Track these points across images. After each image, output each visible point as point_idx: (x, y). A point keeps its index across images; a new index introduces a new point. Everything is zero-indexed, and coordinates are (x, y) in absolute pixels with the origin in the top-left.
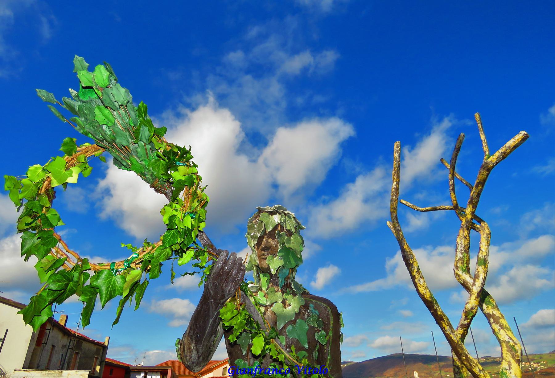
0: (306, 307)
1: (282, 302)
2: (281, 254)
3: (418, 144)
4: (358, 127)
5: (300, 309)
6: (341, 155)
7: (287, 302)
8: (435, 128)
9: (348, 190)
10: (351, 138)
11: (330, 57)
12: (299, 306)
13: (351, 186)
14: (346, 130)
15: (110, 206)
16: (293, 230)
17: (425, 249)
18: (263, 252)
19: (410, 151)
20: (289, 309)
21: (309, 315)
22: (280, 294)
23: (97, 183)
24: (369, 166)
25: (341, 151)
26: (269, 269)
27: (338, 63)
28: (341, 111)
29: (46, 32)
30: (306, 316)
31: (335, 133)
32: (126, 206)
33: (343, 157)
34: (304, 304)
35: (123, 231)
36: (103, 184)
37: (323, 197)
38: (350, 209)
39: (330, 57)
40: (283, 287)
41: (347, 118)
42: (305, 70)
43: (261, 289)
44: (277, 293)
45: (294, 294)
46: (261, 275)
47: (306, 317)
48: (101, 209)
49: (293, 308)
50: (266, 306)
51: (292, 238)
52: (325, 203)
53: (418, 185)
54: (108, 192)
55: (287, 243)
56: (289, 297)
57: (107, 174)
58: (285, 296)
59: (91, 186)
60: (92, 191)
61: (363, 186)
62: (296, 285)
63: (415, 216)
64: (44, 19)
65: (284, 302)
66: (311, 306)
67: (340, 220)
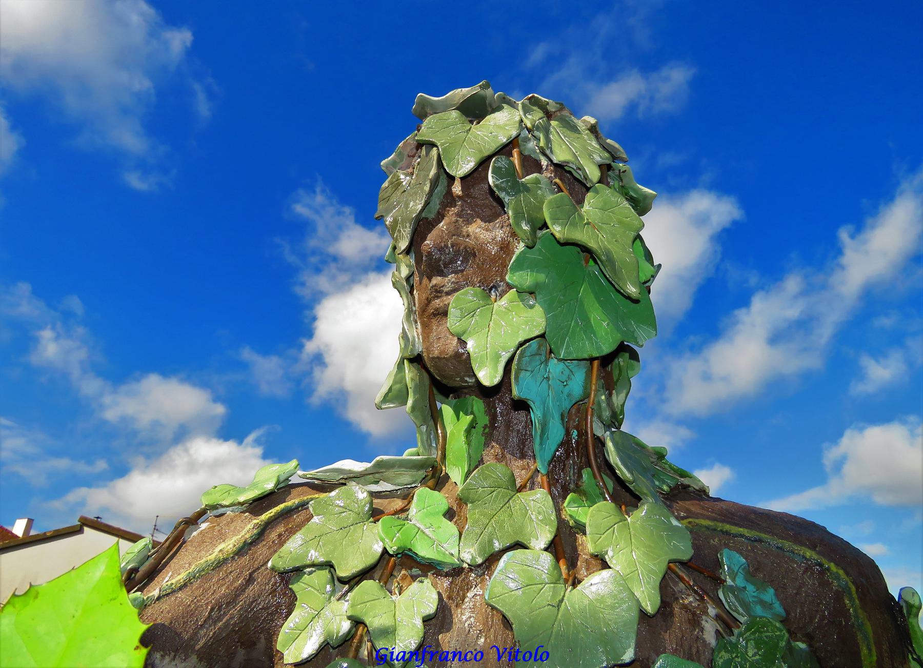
0: (695, 571)
1: (552, 547)
2: (524, 278)
3: (869, 221)
4: (745, 203)
5: (665, 587)
6: (719, 256)
7: (588, 545)
8: (905, 185)
9: (737, 322)
10: (735, 223)
11: (676, 78)
12: (659, 569)
13: (741, 314)
14: (720, 210)
15: (325, 382)
16: (593, 173)
17: (904, 422)
18: (436, 280)
19: (852, 237)
20: (596, 584)
21: (727, 623)
22: (538, 500)
23: (301, 347)
24: (772, 273)
25: (719, 248)
26: (463, 362)
27: (696, 84)
28: (706, 177)
29: (203, 108)
30: (709, 629)
31: (701, 220)
32: (351, 381)
33: (722, 260)
34: (685, 551)
35: (348, 424)
36: (310, 347)
37: (692, 339)
38: (745, 357)
39: (676, 78)
40: (556, 463)
41: (722, 187)
42: (631, 108)
43: (438, 480)
44: (525, 497)
45: (626, 497)
46: (447, 411)
47: (710, 636)
48: (311, 390)
49: (623, 582)
50: (457, 571)
51: (590, 206)
52: (696, 350)
53: (873, 300)
54: (319, 359)
55: (555, 220)
56: (594, 515)
57: (315, 329)
58: (573, 510)
59: (292, 352)
60: (296, 360)
61: (764, 312)
62: (633, 449)
63: (877, 361)
64: (197, 87)
65: (564, 545)
66: (732, 562)
67: (725, 379)
